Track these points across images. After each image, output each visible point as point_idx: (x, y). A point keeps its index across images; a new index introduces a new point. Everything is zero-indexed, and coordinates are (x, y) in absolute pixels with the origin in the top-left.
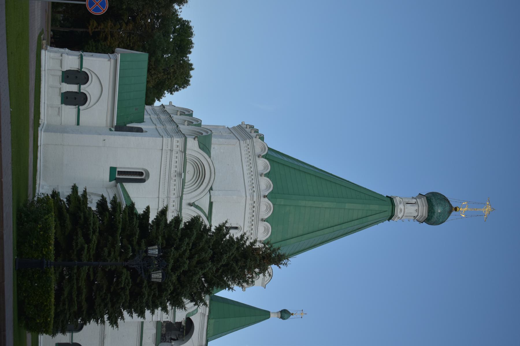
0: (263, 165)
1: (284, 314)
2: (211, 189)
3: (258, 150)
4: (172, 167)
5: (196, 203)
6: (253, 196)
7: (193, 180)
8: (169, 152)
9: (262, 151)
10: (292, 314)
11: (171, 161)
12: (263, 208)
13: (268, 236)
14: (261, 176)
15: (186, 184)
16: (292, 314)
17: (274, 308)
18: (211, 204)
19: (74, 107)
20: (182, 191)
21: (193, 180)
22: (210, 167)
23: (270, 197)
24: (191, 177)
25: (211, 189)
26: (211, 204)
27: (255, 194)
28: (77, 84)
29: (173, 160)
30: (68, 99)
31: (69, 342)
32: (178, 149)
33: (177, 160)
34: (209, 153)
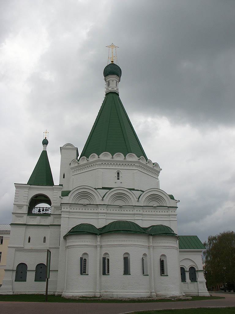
0: (94, 158)
1: (45, 142)
2: (95, 188)
3: (85, 162)
4: (80, 211)
5: (102, 197)
6: (99, 164)
7: (89, 200)
8: (70, 214)
9: (84, 160)
10: (46, 138)
11: (75, 212)
12: (106, 158)
13: (134, 154)
14: (88, 160)
15: (163, 205)
16: (46, 138)
17: (41, 148)
18: (103, 188)
19: (197, 274)
20: (165, 206)
21: (89, 200)
22: (76, 191)
23: (98, 155)
24: (88, 200)
25: (95, 188)
26: (103, 188)
27: (136, 164)
28: (195, 274)
29: (112, 212)
30: (194, 279)
31: (15, 273)
32: (68, 208)
33: (158, 211)
34: (70, 192)
